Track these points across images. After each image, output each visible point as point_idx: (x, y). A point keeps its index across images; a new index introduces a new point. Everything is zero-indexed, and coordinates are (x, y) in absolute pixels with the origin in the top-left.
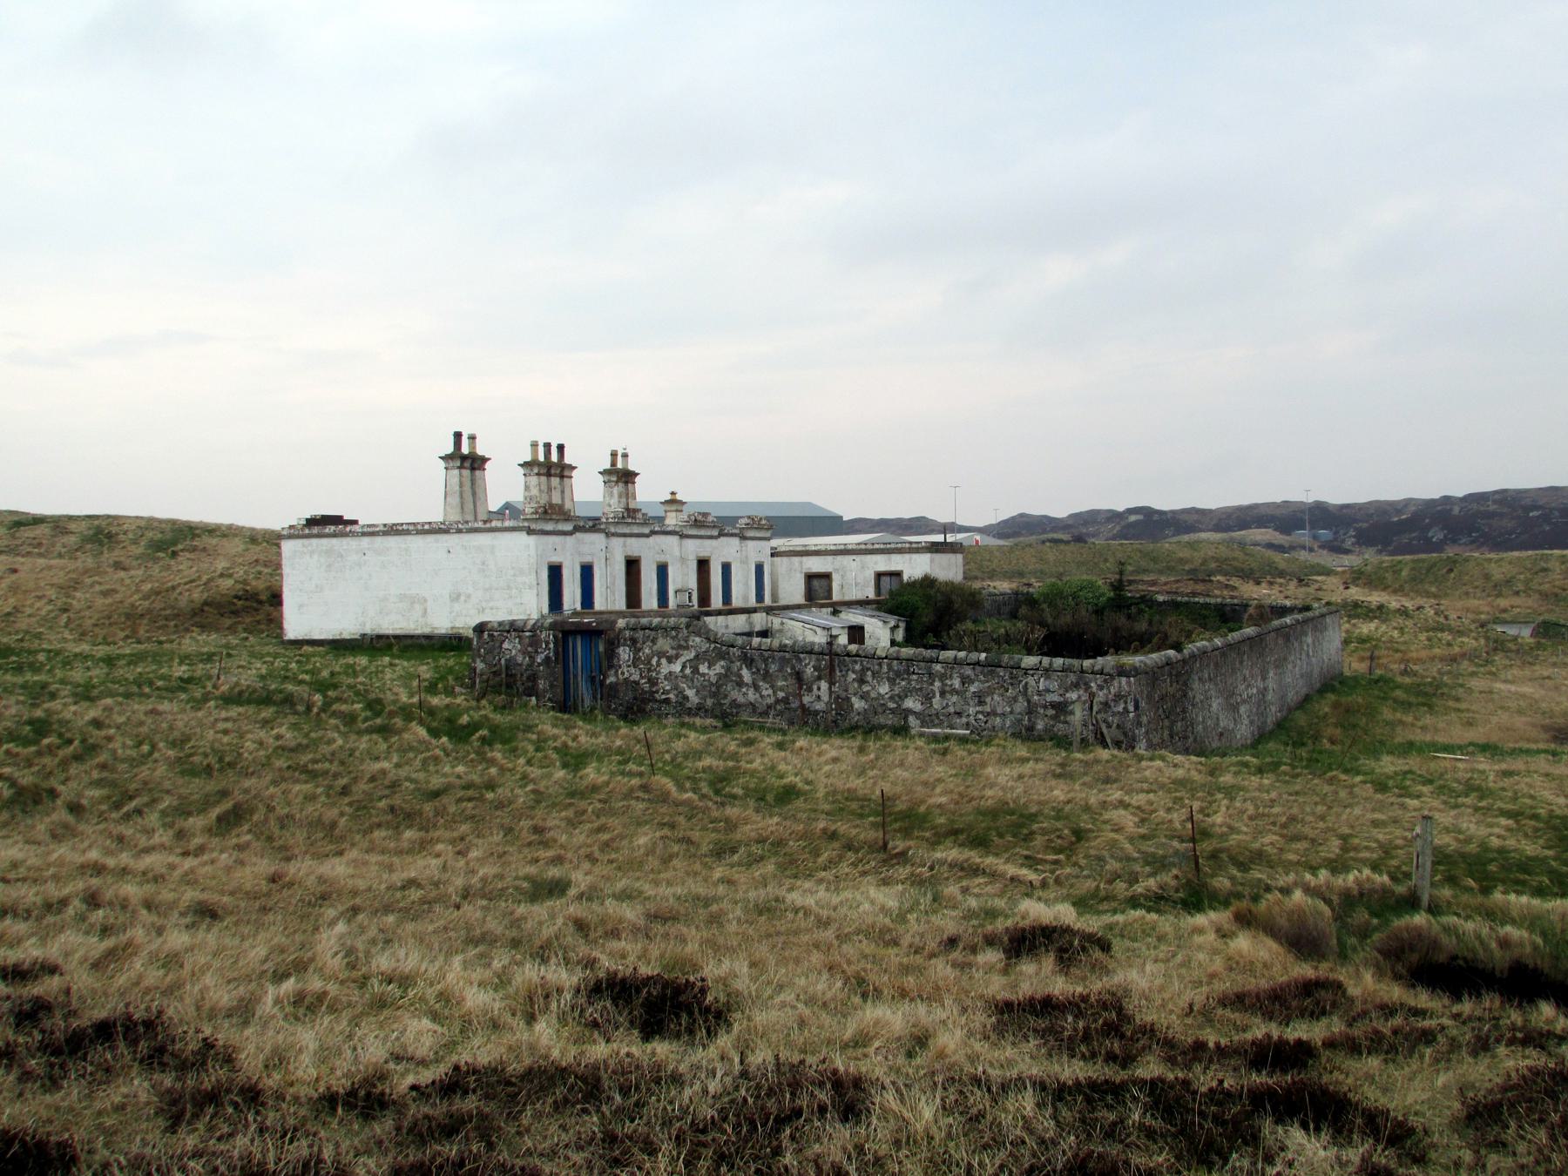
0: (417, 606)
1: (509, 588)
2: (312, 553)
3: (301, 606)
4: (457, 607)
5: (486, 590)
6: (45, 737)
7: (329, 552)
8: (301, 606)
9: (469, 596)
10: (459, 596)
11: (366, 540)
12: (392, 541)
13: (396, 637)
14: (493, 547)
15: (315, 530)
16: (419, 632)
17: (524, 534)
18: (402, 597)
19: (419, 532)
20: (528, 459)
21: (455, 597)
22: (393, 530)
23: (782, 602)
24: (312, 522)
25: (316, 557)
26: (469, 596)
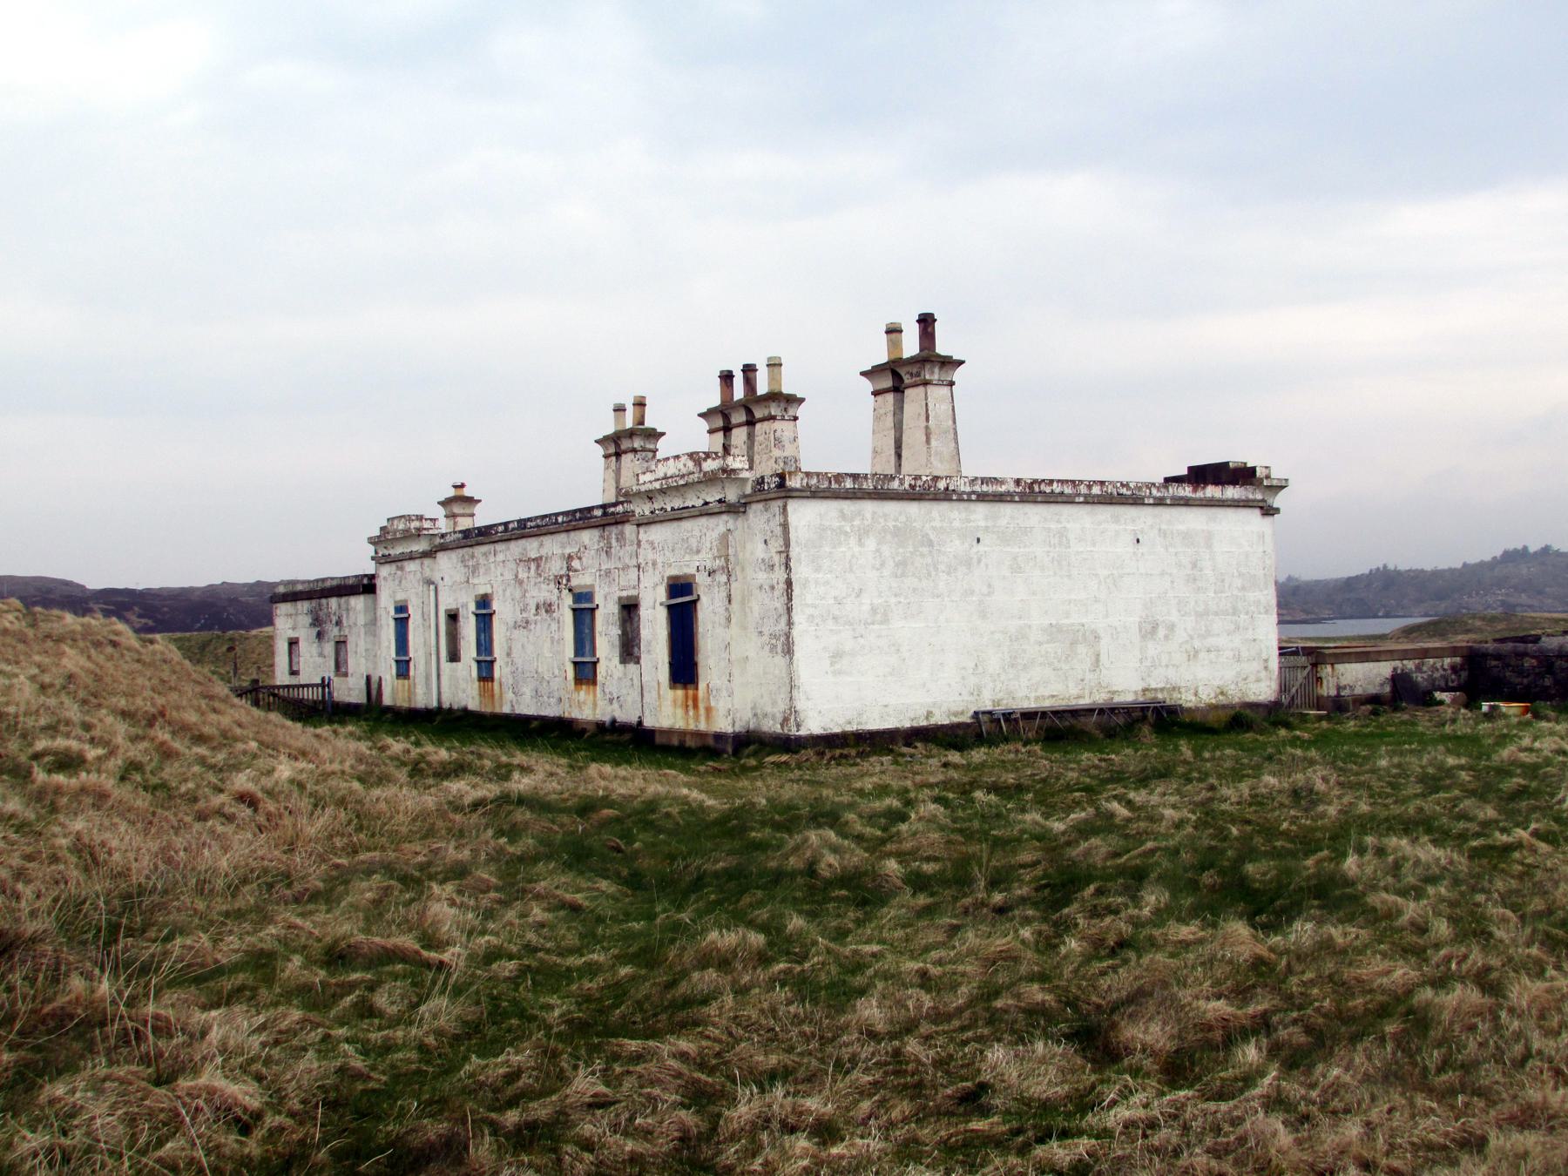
0: (1082, 649)
1: (1235, 612)
2: (862, 535)
3: (837, 656)
4: (1152, 649)
5: (1199, 615)
6: (834, 1144)
7: (900, 534)
8: (837, 656)
9: (1172, 627)
10: (1155, 628)
11: (981, 510)
12: (1034, 514)
13: (1029, 715)
14: (1209, 538)
15: (1212, 491)
16: (1085, 701)
17: (1257, 512)
18: (1054, 631)
19: (1090, 500)
20: (882, 358)
21: (1150, 630)
22: (1032, 493)
23: (304, 606)
24: (1200, 475)
25: (871, 543)
26: (1172, 627)
